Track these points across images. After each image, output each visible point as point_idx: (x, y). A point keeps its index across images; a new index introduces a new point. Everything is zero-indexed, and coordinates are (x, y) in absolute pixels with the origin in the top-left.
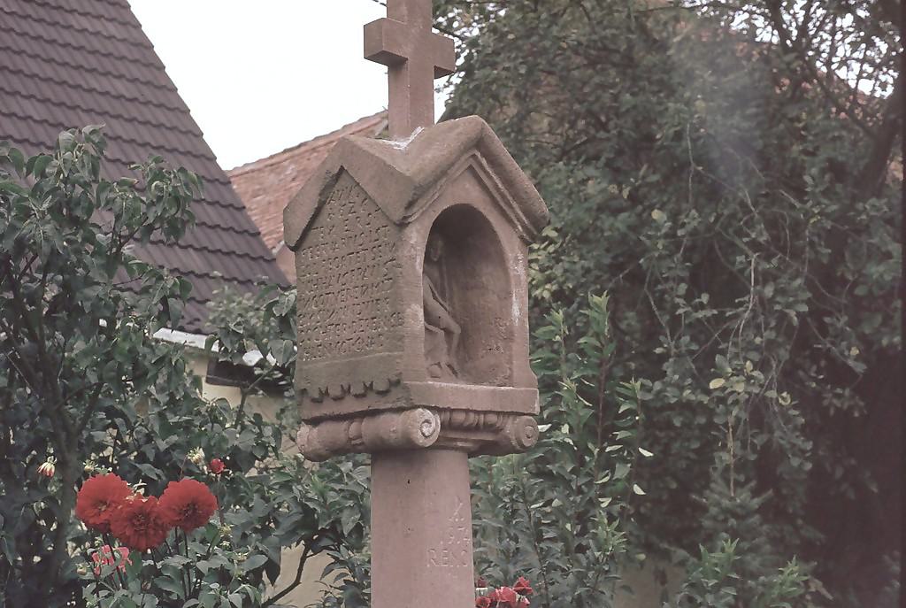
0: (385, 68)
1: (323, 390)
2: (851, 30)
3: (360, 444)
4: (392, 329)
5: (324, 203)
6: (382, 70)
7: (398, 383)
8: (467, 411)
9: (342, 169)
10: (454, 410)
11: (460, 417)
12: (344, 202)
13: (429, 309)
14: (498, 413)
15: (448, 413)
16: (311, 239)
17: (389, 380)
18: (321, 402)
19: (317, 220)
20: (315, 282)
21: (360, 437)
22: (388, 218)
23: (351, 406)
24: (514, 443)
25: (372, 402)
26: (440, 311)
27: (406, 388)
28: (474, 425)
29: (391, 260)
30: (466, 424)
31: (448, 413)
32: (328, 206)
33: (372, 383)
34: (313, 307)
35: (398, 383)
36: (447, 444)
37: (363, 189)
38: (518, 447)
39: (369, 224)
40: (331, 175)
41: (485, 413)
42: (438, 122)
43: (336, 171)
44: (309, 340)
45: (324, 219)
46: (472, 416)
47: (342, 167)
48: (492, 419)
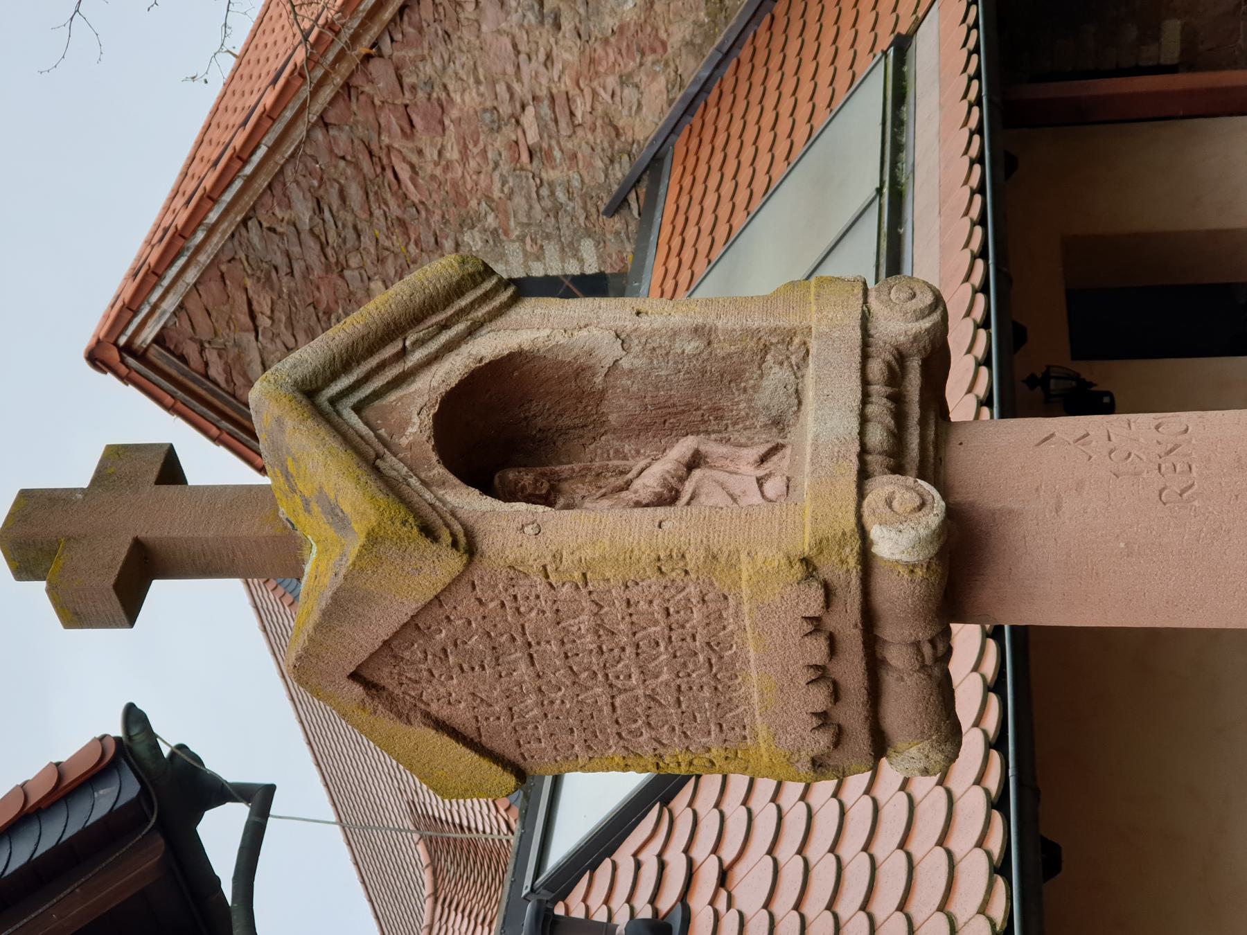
0: (156, 584)
1: (812, 675)
2: (422, 75)
3: (934, 647)
4: (693, 576)
5: (427, 715)
6: (161, 592)
7: (806, 561)
8: (864, 420)
9: (355, 676)
10: (863, 445)
11: (877, 436)
12: (425, 673)
13: (223, 284)
14: (865, 357)
15: (869, 458)
16: (504, 744)
17: (814, 714)
18: (839, 726)
19: (462, 729)
20: (589, 735)
21: (917, 645)
22: (456, 580)
23: (851, 671)
24: (926, 324)
25: (847, 621)
26: (650, 481)
27: (821, 545)
28: (889, 404)
29: (547, 577)
30: (889, 421)
31: (869, 458)
32: (434, 708)
33: (805, 618)
34: (641, 739)
35: (806, 561)
36: (931, 467)
37: (397, 633)
38: (936, 316)
39: (469, 623)
40: (367, 699)
41: (865, 382)
42: (262, 470)
43: (358, 690)
44: (709, 750)
45: (461, 715)
46: (872, 409)
47: (355, 676)
48: (876, 369)
